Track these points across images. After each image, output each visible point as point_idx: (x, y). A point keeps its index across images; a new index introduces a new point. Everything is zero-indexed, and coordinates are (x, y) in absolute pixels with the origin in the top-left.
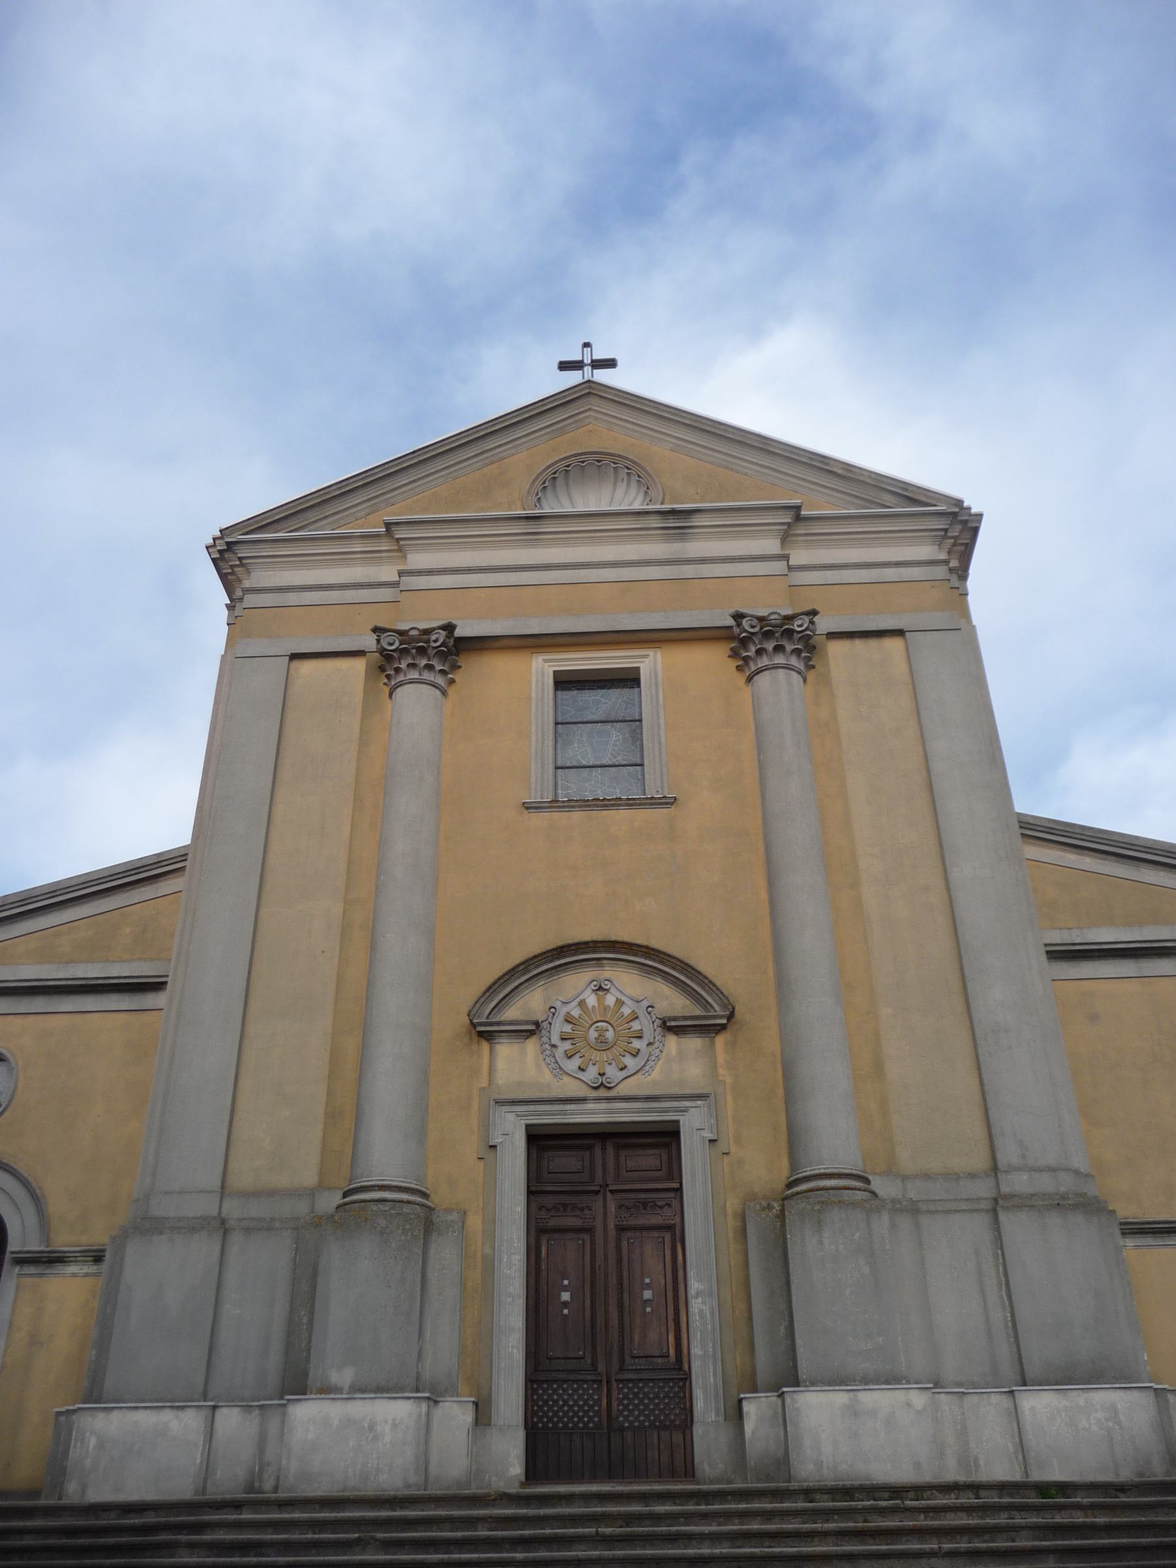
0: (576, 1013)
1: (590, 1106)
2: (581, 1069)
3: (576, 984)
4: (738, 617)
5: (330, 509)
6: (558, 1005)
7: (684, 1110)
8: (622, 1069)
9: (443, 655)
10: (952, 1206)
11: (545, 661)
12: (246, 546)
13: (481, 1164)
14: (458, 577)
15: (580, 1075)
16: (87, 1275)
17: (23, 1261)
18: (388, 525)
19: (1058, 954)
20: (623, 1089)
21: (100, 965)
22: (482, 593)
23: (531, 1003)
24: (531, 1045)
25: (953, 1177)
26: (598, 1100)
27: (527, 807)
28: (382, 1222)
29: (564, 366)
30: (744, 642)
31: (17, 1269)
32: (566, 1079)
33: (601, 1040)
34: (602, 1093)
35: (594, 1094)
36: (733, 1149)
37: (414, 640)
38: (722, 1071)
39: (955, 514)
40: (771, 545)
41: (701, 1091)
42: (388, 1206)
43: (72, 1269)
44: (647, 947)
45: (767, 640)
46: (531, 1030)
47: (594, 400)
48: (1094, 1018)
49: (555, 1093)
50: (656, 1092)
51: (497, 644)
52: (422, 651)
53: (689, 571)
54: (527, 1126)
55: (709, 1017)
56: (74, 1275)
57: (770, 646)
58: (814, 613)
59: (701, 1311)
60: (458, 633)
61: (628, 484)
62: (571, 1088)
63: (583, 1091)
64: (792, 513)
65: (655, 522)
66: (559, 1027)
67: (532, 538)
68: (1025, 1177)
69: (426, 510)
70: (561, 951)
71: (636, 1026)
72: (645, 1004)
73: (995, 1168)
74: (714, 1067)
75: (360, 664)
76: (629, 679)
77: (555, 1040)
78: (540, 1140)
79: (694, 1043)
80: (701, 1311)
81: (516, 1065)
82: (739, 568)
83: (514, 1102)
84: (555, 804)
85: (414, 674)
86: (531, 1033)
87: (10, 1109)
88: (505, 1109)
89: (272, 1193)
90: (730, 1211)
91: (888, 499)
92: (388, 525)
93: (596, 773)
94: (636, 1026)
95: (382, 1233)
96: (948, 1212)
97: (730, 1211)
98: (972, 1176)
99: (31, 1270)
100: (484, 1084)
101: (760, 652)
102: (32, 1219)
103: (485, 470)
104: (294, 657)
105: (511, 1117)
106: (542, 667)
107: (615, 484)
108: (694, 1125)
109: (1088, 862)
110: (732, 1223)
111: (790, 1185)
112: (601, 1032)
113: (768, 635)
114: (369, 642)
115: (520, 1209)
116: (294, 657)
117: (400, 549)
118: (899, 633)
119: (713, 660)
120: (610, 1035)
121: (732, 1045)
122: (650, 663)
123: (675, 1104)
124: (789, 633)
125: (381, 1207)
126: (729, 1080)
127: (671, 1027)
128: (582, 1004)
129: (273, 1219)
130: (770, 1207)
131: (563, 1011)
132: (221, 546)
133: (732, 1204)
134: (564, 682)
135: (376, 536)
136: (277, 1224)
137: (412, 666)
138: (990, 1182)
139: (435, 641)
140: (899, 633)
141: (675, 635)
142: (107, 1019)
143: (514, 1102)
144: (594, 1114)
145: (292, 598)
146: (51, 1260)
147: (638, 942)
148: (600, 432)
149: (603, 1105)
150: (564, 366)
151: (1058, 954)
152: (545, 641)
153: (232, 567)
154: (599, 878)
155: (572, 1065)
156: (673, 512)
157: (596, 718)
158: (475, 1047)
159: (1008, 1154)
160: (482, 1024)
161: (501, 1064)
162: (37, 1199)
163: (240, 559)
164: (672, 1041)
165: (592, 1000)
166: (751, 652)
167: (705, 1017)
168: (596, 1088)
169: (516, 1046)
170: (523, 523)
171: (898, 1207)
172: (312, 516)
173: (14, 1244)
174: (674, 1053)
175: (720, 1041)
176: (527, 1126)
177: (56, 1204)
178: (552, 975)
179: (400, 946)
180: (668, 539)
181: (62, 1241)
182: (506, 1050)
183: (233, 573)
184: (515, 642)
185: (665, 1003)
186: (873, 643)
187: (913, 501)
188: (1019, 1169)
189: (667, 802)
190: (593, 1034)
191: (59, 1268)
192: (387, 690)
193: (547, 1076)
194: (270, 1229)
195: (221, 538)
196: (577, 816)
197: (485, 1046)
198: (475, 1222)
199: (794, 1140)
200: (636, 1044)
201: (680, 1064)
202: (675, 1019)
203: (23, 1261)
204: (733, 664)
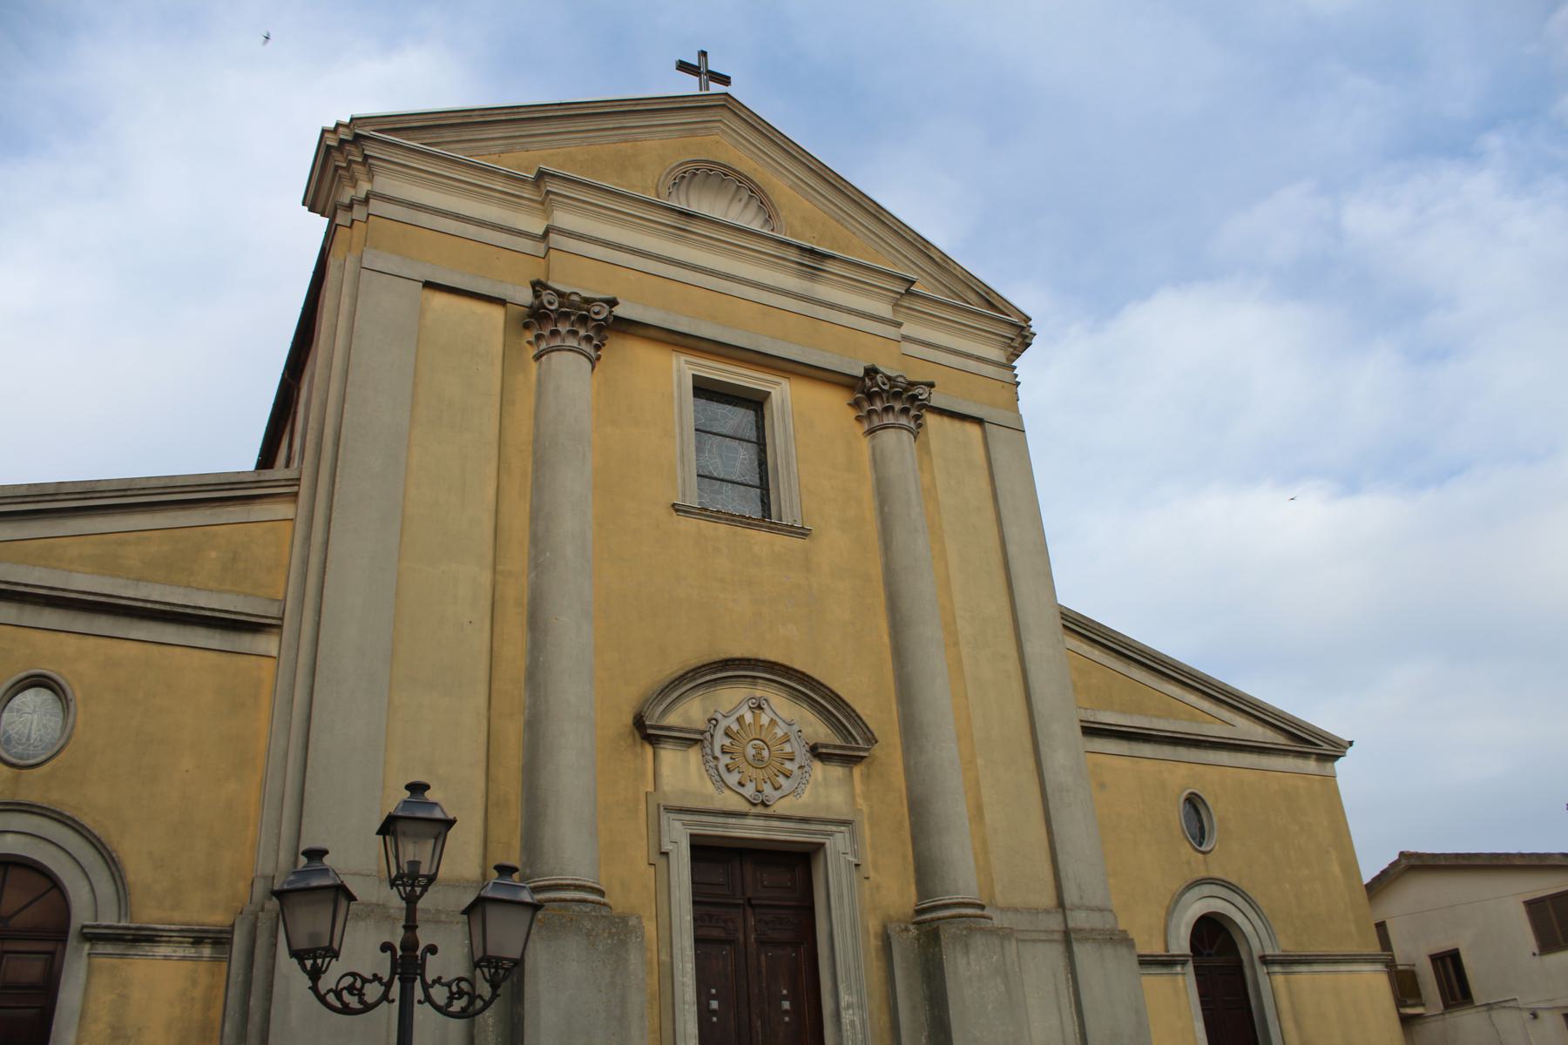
0: (735, 727)
1: (749, 821)
2: (741, 784)
3: (731, 698)
4: (871, 372)
5: (467, 134)
6: (719, 717)
7: (831, 834)
8: (776, 789)
9: (600, 328)
10: (1035, 936)
11: (687, 362)
12: (376, 145)
13: (652, 869)
14: (605, 252)
15: (740, 790)
16: (184, 958)
17: (92, 937)
18: (541, 175)
19: (1091, 731)
20: (780, 807)
21: (181, 590)
22: (632, 275)
23: (690, 711)
24: (694, 755)
25: (1034, 911)
26: (757, 816)
27: (676, 508)
28: (588, 924)
29: (683, 66)
30: (870, 397)
31: (87, 946)
32: (727, 793)
33: (758, 758)
34: (760, 810)
35: (754, 810)
36: (872, 874)
37: (572, 305)
38: (860, 801)
39: (1023, 328)
40: (884, 309)
41: (844, 818)
42: (587, 908)
43: (163, 950)
44: (803, 673)
45: (883, 398)
46: (690, 740)
47: (726, 116)
48: (1102, 786)
49: (718, 805)
50: (808, 814)
51: (641, 332)
52: (583, 320)
53: (822, 312)
54: (692, 836)
55: (847, 746)
56: (166, 958)
57: (898, 406)
58: (931, 385)
59: (852, 1022)
60: (618, 311)
61: (746, 205)
62: (733, 802)
63: (743, 806)
64: (906, 285)
65: (793, 255)
66: (720, 740)
67: (680, 233)
68: (1083, 914)
69: (562, 167)
70: (726, 664)
71: (787, 748)
72: (796, 728)
73: (1061, 904)
74: (853, 797)
75: (497, 313)
76: (755, 402)
77: (718, 753)
78: (705, 851)
79: (836, 771)
80: (852, 1022)
81: (680, 772)
82: (855, 323)
83: (681, 810)
84: (703, 512)
85: (572, 342)
86: (696, 741)
87: (67, 749)
88: (672, 816)
89: (1016, 910)
90: (872, 931)
91: (972, 297)
92: (541, 175)
93: (727, 487)
94: (787, 748)
95: (588, 935)
96: (1034, 941)
97: (872, 931)
98: (1047, 911)
99: (109, 948)
100: (650, 788)
101: (887, 410)
102: (105, 887)
103: (621, 146)
104: (428, 285)
105: (678, 825)
106: (684, 368)
107: (731, 201)
108: (837, 844)
109: (1096, 654)
110: (874, 943)
111: (919, 912)
112: (759, 750)
113: (897, 396)
114: (525, 296)
115: (689, 918)
116: (428, 285)
117: (546, 203)
118: (979, 421)
119: (832, 404)
120: (765, 753)
121: (867, 777)
122: (782, 392)
123: (822, 827)
124: (914, 398)
125: (582, 907)
126: (865, 809)
127: (818, 753)
128: (740, 720)
129: (438, 911)
130: (907, 930)
131: (723, 724)
132: (345, 134)
133: (874, 925)
134: (705, 390)
135: (523, 180)
136: (443, 917)
137: (574, 333)
138: (1060, 918)
139: (597, 313)
140: (979, 421)
141: (805, 370)
142: (193, 659)
143: (681, 810)
144: (752, 829)
145: (424, 219)
146: (142, 938)
147: (796, 667)
148: (727, 147)
149: (761, 823)
150: (683, 66)
151: (1091, 731)
152: (688, 341)
153: (351, 162)
154: (742, 592)
155: (732, 779)
156: (812, 252)
157: (724, 432)
158: (639, 749)
159: (1071, 897)
160: (652, 727)
161: (666, 770)
162: (111, 862)
163: (366, 157)
164: (818, 768)
165: (749, 718)
166: (878, 406)
167: (852, 749)
168: (755, 805)
169: (680, 754)
170: (675, 216)
171: (993, 932)
172: (449, 135)
173: (81, 915)
174: (820, 778)
175: (857, 771)
176: (692, 836)
177: (137, 869)
178: (796, 697)
179: (573, 635)
180: (802, 275)
181: (148, 915)
182: (670, 756)
183: (347, 169)
184: (663, 336)
185: (810, 730)
186: (957, 424)
187: (991, 305)
188: (1079, 908)
189: (803, 533)
190: (750, 752)
191: (146, 948)
192: (533, 352)
193: (710, 788)
194: (437, 922)
195: (346, 126)
196: (723, 529)
197: (649, 750)
198: (650, 927)
199: (925, 871)
200: (788, 765)
201: (821, 791)
202: (826, 746)
203: (92, 937)
204: (852, 413)
